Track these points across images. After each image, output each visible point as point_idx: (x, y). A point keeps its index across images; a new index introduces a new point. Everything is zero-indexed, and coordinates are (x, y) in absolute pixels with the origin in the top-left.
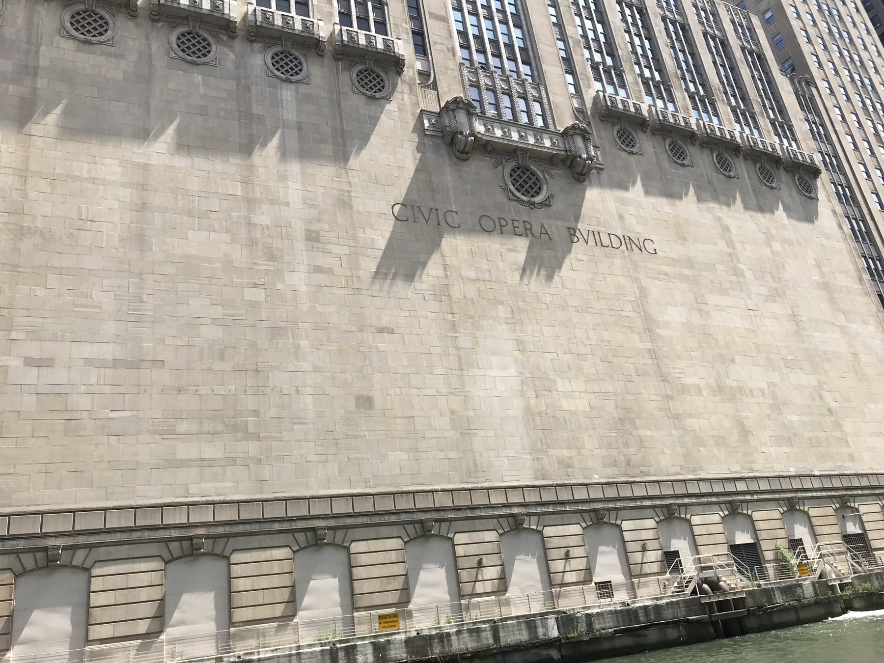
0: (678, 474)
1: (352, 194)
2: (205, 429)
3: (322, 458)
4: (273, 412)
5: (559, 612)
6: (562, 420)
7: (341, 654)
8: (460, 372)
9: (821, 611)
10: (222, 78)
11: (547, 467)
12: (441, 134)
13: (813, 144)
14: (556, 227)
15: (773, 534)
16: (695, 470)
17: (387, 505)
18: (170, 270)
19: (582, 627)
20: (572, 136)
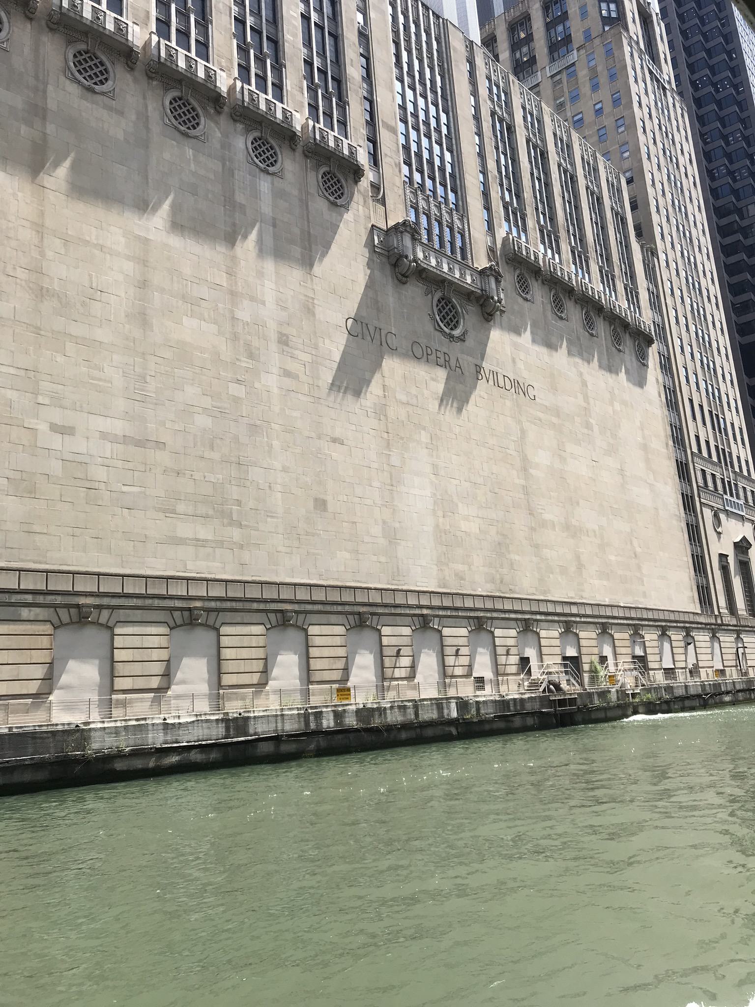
1: (315, 301)
2: (199, 512)
3: (288, 550)
4: (251, 504)
5: (458, 698)
6: (460, 539)
7: (312, 718)
8: (390, 488)
9: (620, 712)
10: (210, 156)
11: (447, 578)
12: (386, 253)
13: (650, 312)
14: (467, 361)
15: (590, 650)
16: (544, 593)
17: (334, 596)
18: (168, 354)
19: (473, 711)
20: (402, 232)
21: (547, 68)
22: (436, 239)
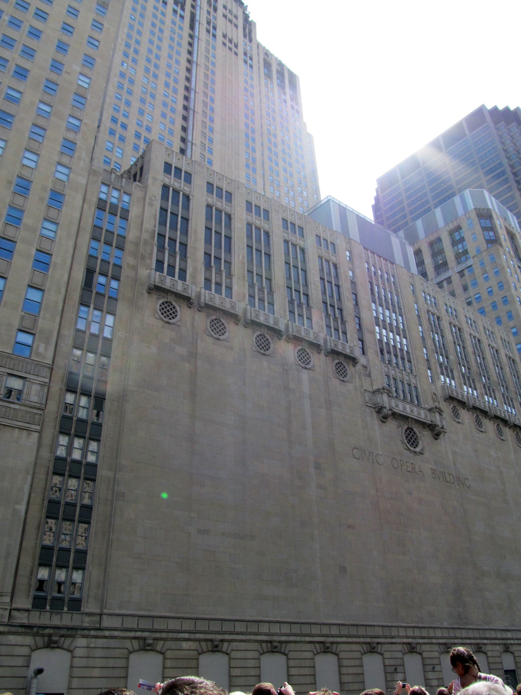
0: (481, 625)
20: (434, 412)
21: (455, 268)
22: (401, 392)
